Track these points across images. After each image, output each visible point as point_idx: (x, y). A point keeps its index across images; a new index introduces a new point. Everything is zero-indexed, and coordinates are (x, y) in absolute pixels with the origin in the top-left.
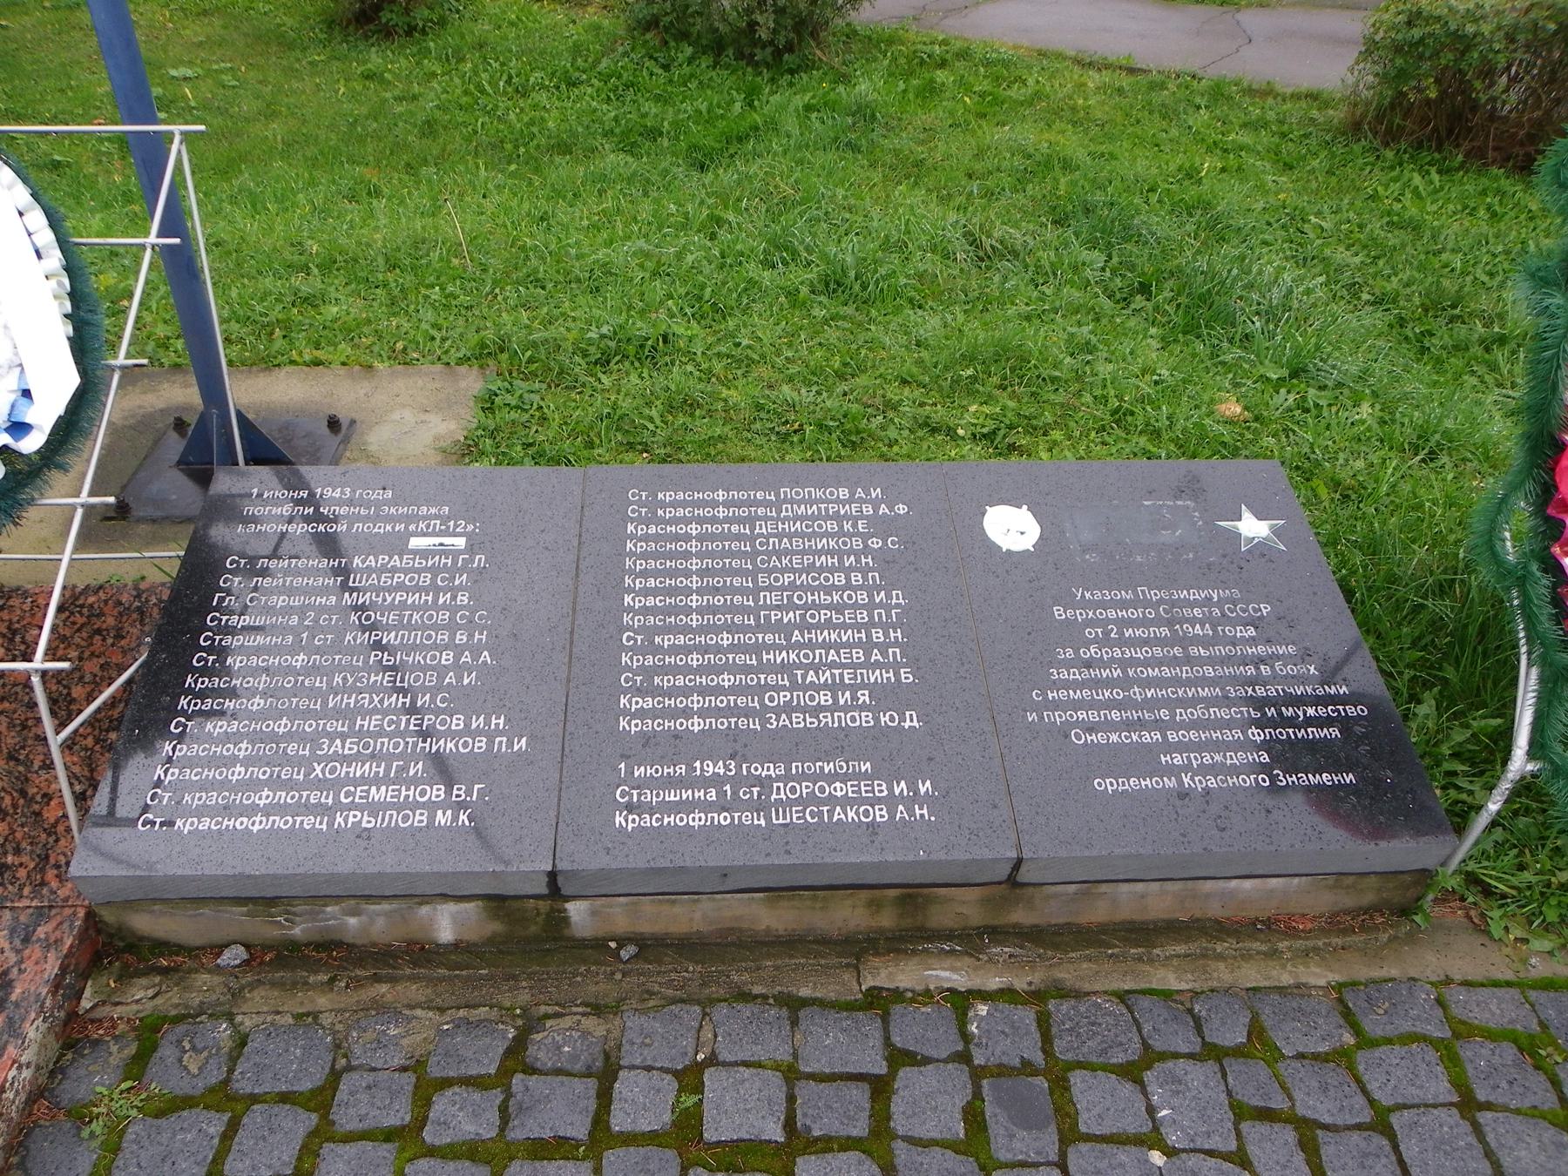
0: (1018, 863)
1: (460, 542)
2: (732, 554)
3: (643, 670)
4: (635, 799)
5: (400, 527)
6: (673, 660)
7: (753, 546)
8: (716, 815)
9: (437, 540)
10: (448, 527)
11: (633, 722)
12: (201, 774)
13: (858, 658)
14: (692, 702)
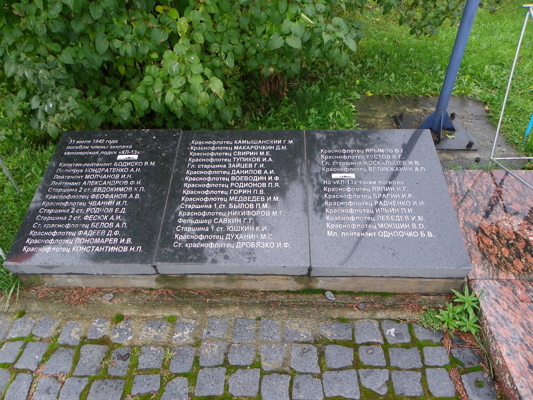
0: (310, 269)
1: (136, 157)
2: (225, 151)
3: (194, 163)
4: (186, 207)
5: (115, 153)
6: (197, 214)
7: (232, 154)
8: (207, 236)
9: (127, 156)
10: (131, 153)
11: (180, 236)
12: (44, 233)
13: (263, 200)
14: (200, 237)
